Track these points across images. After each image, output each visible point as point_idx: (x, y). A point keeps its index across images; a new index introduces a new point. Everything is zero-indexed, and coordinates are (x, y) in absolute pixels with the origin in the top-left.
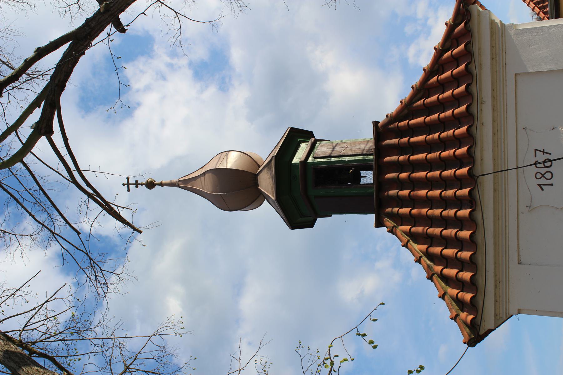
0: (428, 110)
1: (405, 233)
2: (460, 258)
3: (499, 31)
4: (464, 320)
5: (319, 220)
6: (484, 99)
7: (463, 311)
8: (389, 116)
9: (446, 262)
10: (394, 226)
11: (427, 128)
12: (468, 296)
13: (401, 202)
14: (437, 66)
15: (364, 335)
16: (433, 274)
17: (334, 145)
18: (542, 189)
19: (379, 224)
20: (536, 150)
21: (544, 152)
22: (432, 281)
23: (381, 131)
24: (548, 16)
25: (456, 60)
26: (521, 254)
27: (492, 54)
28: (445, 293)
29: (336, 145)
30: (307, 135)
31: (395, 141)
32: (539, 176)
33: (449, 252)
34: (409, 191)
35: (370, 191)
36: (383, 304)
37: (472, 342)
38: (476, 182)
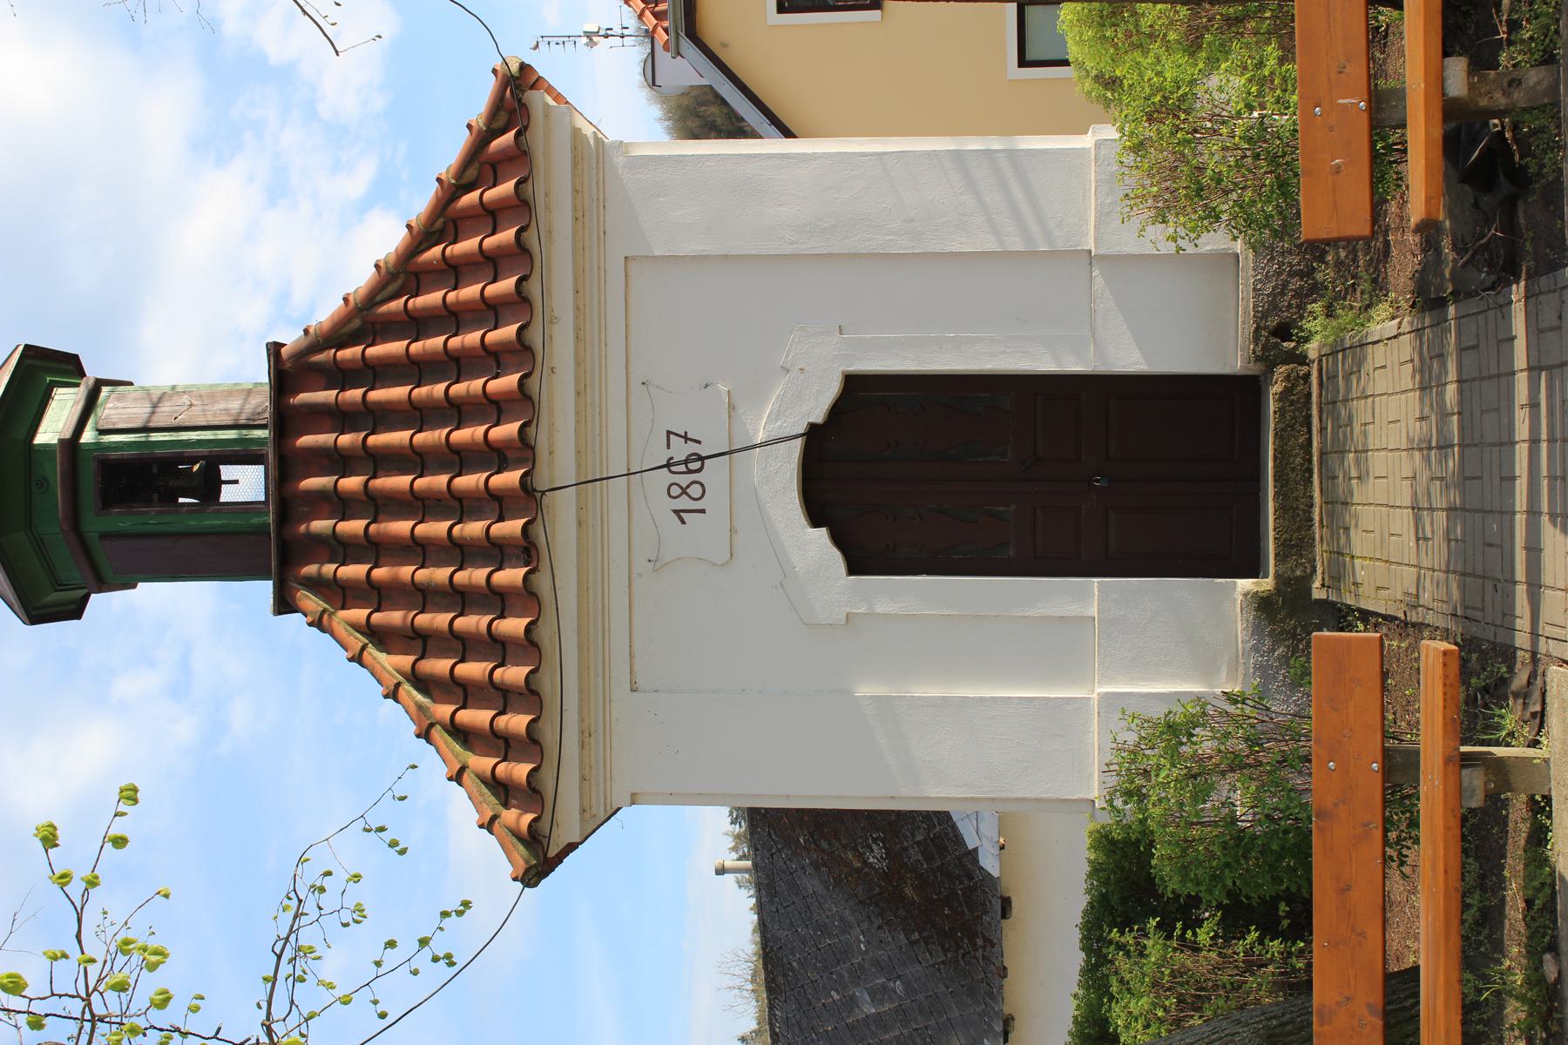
0: (417, 325)
1: (356, 627)
2: (502, 682)
3: (590, 155)
4: (513, 826)
5: (95, 598)
6: (556, 313)
7: (506, 805)
8: (312, 331)
9: (465, 693)
10: (324, 611)
11: (416, 370)
12: (520, 771)
13: (344, 550)
14: (441, 220)
15: (382, 829)
16: (432, 725)
17: (155, 399)
18: (683, 522)
19: (284, 605)
20: (669, 433)
21: (686, 438)
22: (429, 741)
23: (288, 371)
24: (666, 24)
25: (492, 216)
26: (636, 668)
27: (575, 209)
28: (462, 769)
29: (160, 399)
30: (67, 366)
31: (327, 396)
32: (675, 491)
33: (473, 669)
34: (365, 522)
35: (256, 520)
36: (414, 767)
37: (532, 876)
38: (538, 505)
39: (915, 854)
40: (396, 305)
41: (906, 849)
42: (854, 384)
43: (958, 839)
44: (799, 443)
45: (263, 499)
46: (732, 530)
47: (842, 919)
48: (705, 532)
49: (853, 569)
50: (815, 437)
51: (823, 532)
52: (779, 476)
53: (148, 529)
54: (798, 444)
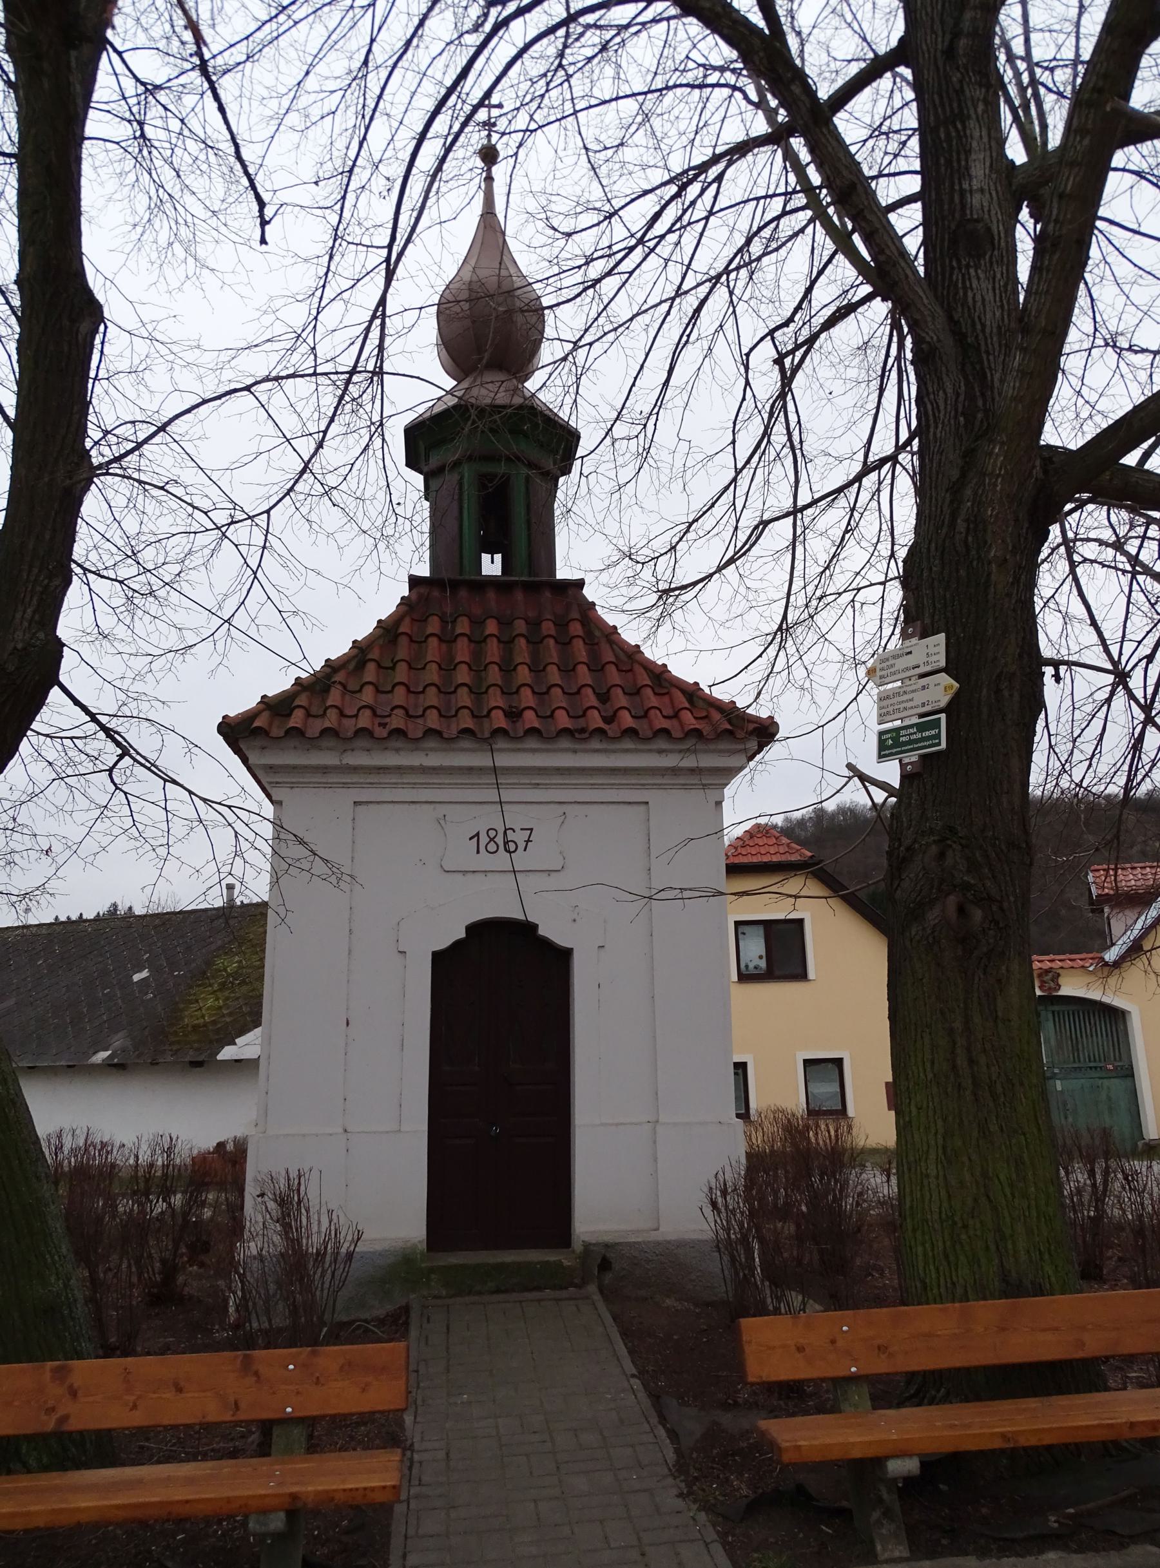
18: (471, 839)
20: (531, 830)
21: (528, 841)
32: (492, 834)
42: (564, 956)
44: (523, 918)
47: (194, 960)
48: (465, 855)
49: (436, 956)
51: (463, 935)
52: (497, 902)
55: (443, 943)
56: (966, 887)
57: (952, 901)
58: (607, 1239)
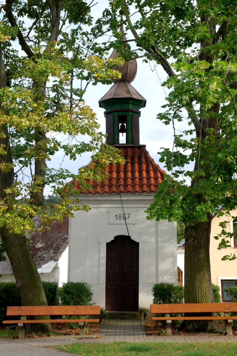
21: (129, 217)
32: (120, 215)
39: (40, 254)
40: (151, 169)
41: (41, 252)
42: (137, 244)
43: (44, 264)
44: (128, 235)
45: (120, 143)
46: (114, 224)
48: (113, 220)
49: (108, 244)
50: (129, 238)
53: (115, 124)
54: (127, 235)
55: (109, 241)
56: (194, 237)
57: (192, 239)
58: (146, 309)
